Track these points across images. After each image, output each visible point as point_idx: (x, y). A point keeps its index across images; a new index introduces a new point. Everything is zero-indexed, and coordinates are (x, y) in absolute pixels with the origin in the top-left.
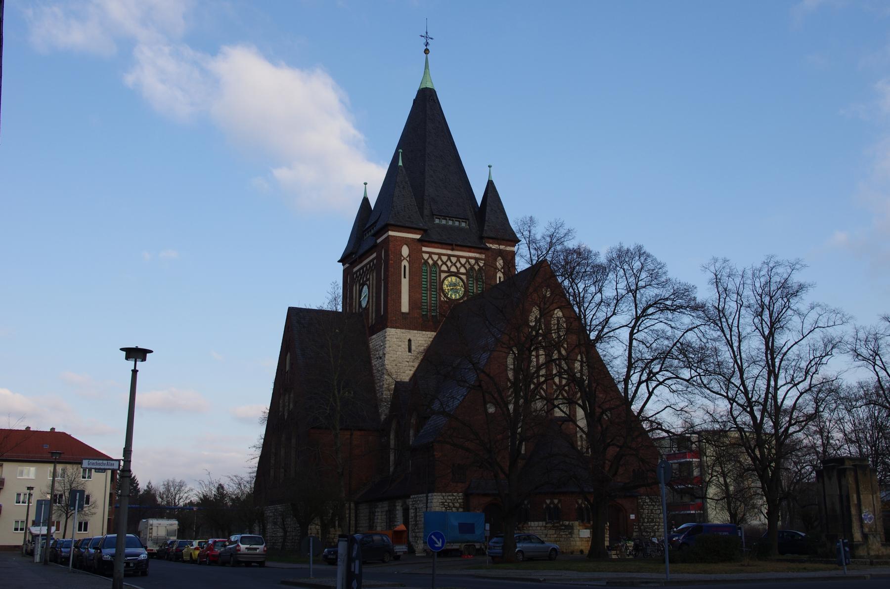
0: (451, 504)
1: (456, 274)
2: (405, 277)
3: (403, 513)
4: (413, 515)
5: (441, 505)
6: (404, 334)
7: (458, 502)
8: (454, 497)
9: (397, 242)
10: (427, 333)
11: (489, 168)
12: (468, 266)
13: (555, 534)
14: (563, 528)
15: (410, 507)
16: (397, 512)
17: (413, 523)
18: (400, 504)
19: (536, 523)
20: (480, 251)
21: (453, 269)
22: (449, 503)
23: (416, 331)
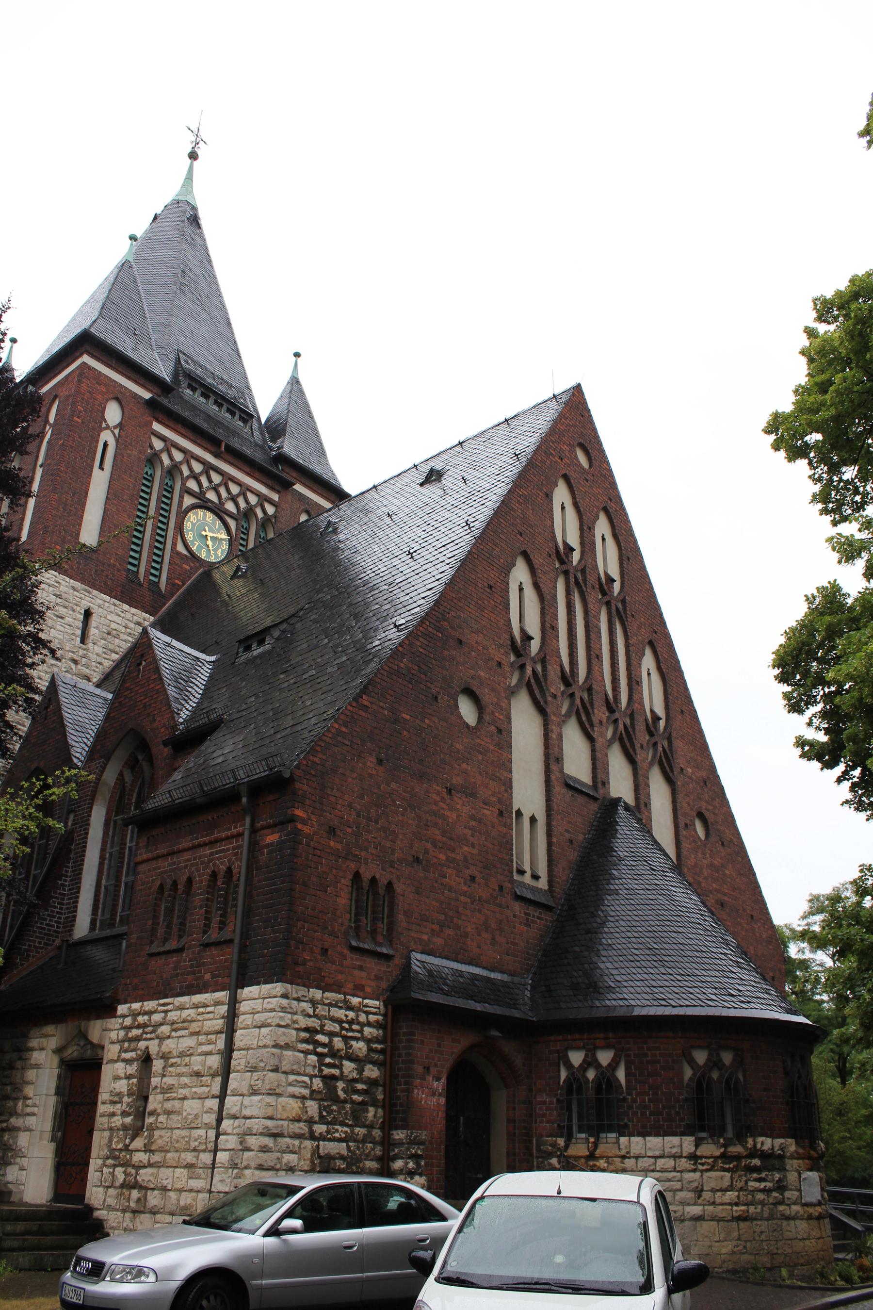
0: (338, 1043)
1: (218, 511)
2: (101, 467)
3: (59, 1077)
4: (122, 1086)
5: (306, 1041)
6: (76, 593)
7: (363, 1039)
8: (351, 1015)
9: (99, 385)
10: (134, 610)
11: (294, 358)
12: (242, 505)
13: (731, 1188)
14: (756, 1162)
15: (111, 1051)
16: (31, 1074)
17: (117, 1121)
18: (53, 1043)
19: (654, 1142)
20: (269, 482)
21: (211, 496)
22: (331, 1034)
23: (107, 598)
